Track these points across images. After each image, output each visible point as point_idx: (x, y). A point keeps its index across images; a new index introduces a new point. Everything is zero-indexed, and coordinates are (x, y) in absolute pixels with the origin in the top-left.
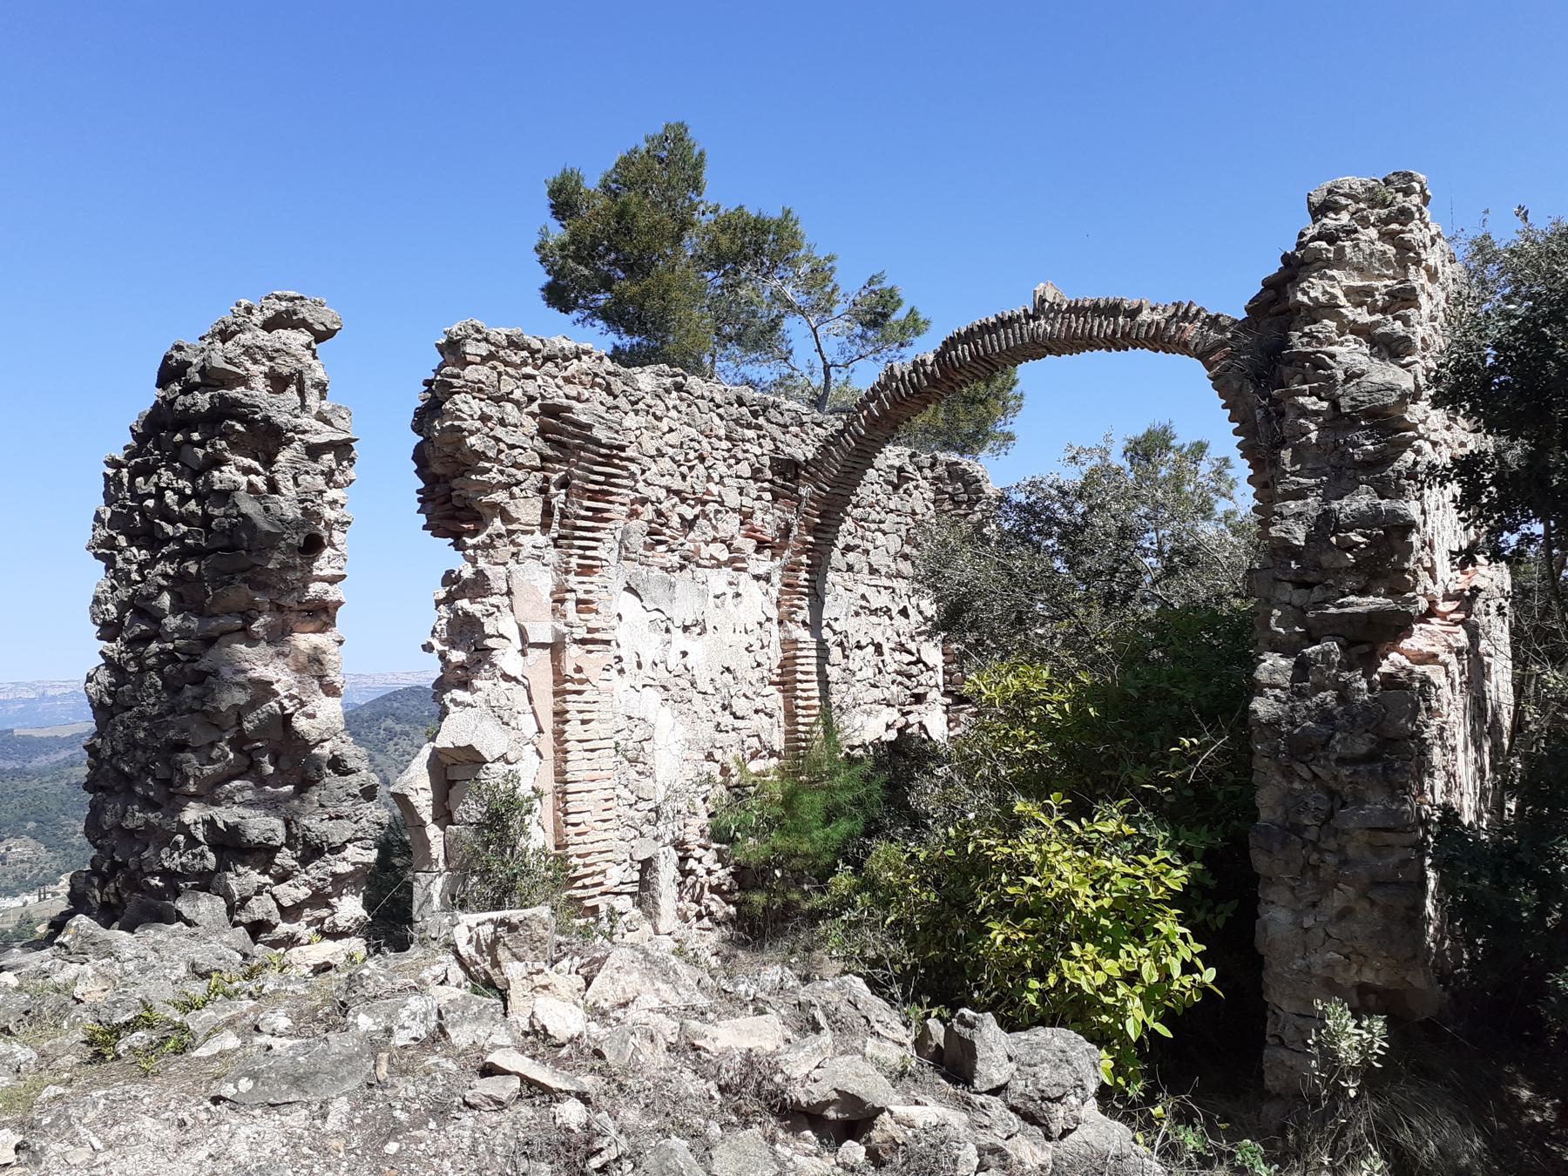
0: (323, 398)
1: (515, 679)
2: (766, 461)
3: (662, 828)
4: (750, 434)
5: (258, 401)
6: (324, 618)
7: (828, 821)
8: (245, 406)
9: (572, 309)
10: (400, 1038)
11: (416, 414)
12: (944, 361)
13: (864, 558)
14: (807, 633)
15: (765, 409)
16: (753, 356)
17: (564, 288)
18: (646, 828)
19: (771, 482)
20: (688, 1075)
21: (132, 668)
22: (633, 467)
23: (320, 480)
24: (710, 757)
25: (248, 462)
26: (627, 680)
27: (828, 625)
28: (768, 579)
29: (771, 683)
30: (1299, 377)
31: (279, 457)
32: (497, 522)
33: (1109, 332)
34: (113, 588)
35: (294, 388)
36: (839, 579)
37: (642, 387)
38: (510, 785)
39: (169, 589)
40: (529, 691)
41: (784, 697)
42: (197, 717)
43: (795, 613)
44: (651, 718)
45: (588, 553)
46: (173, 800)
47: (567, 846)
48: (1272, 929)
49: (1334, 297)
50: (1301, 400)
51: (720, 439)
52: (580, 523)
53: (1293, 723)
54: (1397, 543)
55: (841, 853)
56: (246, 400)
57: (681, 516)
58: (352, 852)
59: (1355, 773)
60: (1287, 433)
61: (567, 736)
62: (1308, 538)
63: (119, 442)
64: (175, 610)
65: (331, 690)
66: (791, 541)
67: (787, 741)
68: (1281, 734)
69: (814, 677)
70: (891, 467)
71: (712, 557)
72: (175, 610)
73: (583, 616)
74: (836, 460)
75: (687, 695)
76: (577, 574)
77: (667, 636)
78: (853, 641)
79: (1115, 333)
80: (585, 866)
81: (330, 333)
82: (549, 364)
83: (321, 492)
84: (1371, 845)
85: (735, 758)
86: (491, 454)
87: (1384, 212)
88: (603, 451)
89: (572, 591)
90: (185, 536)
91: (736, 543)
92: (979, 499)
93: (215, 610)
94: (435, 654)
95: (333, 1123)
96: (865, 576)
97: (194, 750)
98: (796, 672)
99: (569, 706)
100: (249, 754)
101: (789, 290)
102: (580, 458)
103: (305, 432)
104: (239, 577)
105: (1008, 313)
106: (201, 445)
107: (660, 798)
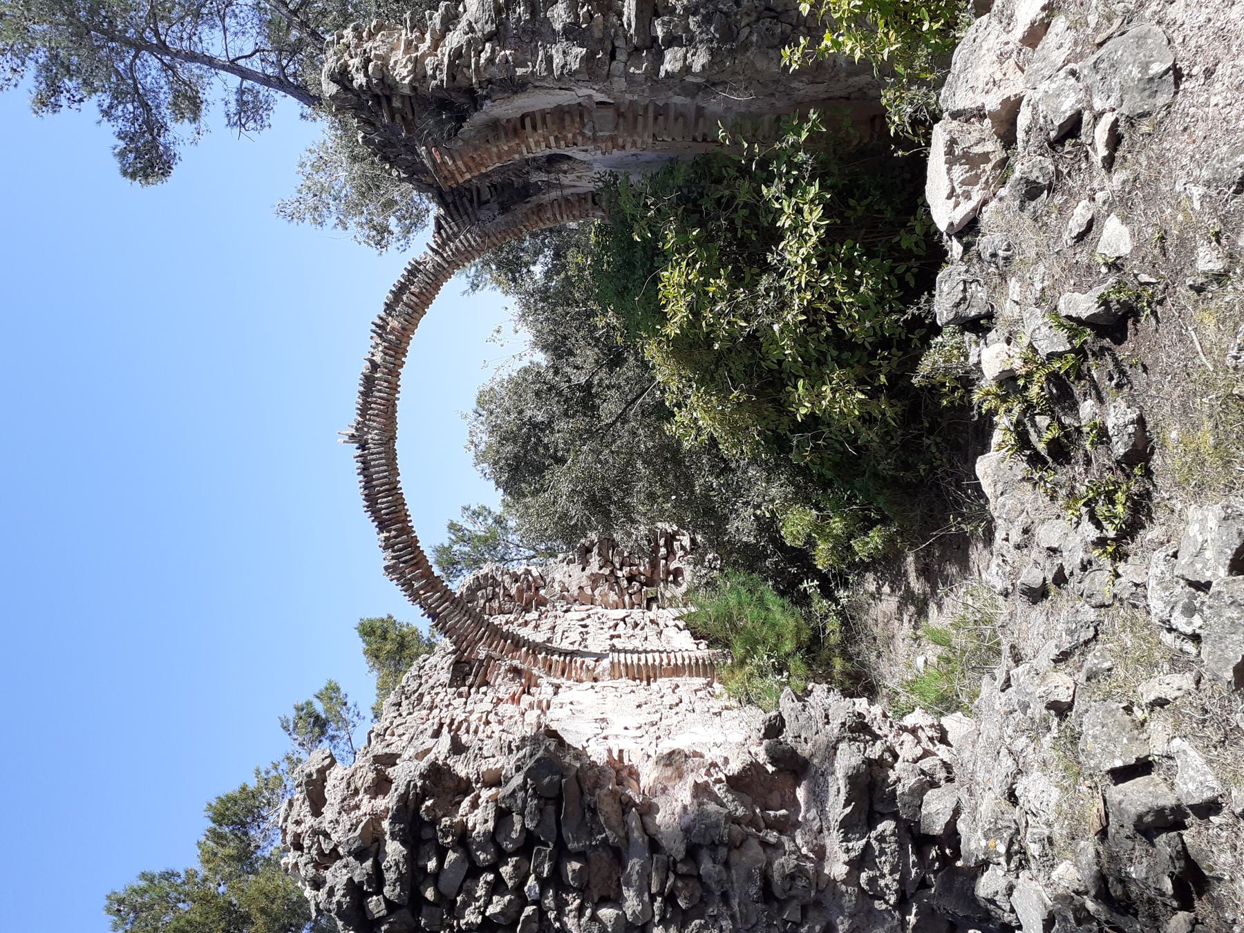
8: (407, 792)
12: (390, 520)
19: (470, 687)
28: (558, 687)
30: (465, 70)
31: (463, 774)
33: (386, 384)
39: (597, 906)
41: (661, 677)
43: (587, 667)
53: (711, 41)
64: (616, 900)
66: (524, 667)
67: (698, 675)
72: (616, 900)
74: (458, 621)
92: (493, 577)
93: (622, 834)
98: (638, 665)
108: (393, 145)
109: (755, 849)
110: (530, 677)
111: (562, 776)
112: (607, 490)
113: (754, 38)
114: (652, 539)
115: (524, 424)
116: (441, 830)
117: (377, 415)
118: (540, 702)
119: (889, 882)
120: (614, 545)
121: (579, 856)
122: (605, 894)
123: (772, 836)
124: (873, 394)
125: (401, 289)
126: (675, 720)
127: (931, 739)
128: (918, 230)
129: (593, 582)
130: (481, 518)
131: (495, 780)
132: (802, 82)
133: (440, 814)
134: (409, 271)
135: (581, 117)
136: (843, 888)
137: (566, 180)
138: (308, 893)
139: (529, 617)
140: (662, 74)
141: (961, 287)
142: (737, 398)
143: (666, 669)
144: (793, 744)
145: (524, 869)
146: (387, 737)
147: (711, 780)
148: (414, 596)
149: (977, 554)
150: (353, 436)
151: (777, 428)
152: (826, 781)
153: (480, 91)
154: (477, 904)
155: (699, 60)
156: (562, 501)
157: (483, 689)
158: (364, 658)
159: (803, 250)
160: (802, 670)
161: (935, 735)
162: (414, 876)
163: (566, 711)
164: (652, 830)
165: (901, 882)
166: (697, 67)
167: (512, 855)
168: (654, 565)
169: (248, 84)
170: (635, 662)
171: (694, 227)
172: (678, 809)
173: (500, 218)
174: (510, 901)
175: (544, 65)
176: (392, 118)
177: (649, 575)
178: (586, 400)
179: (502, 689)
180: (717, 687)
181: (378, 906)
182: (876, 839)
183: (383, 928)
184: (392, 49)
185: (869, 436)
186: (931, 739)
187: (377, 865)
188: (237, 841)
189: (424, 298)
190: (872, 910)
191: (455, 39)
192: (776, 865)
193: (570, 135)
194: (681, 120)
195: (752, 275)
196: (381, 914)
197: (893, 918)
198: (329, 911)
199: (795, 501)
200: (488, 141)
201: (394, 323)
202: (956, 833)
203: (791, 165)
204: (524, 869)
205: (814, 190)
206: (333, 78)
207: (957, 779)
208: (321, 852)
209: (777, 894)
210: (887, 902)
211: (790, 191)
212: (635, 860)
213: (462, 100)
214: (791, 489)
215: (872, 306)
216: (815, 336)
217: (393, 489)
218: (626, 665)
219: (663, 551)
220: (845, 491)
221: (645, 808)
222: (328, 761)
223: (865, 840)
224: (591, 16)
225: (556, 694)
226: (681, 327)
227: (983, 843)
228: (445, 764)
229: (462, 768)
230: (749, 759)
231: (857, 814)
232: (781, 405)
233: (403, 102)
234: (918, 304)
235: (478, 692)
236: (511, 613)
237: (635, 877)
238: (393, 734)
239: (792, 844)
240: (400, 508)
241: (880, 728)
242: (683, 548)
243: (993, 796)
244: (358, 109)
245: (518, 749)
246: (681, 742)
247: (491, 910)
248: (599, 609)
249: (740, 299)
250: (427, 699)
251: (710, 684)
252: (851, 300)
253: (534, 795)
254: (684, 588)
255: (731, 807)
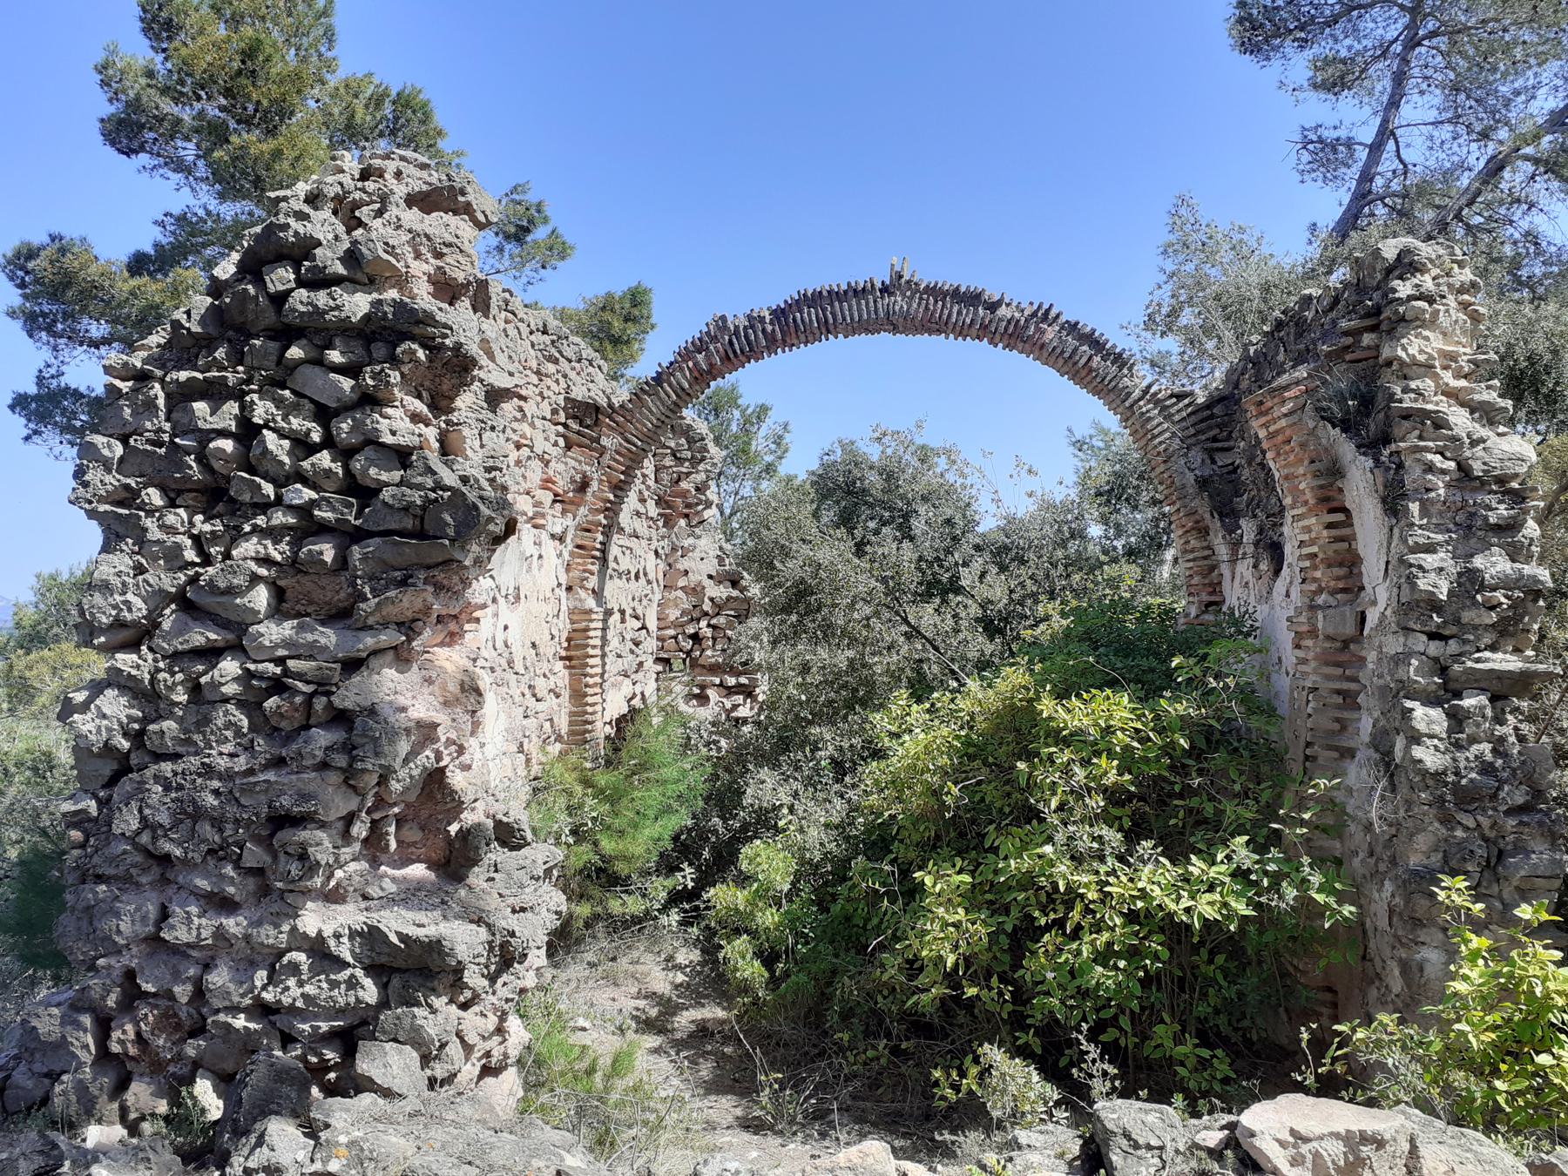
8: (436, 324)
19: (565, 425)
28: (561, 539)
30: (1417, 432)
31: (459, 403)
33: (968, 321)
39: (273, 585)
53: (1457, 774)
59: (1521, 823)
62: (1451, 593)
64: (281, 606)
67: (571, 723)
68: (1446, 784)
72: (281, 606)
92: (703, 459)
93: (371, 621)
108: (1299, 335)
109: (342, 804)
110: (577, 504)
111: (452, 541)
112: (819, 610)
113: (1459, 833)
114: (747, 667)
115: (909, 504)
116: (382, 370)
117: (927, 308)
118: (543, 516)
119: (292, 993)
120: (742, 617)
121: (342, 561)
122: (289, 594)
123: (360, 830)
124: (952, 979)
125: (1096, 344)
126: (516, 693)
127: (488, 1054)
128: (1181, 1049)
129: (694, 589)
130: (773, 447)
131: (447, 449)
132: (1393, 896)
133: (405, 369)
134: (1120, 355)
135: (1344, 590)
136: (286, 928)
137: (1244, 568)
138: (302, 188)
139: (651, 504)
140: (1409, 704)
141: (1155, 1142)
142: (948, 793)
143: (580, 681)
144: (486, 861)
145: (327, 484)
146: (504, 314)
147: (440, 746)
148: (685, 354)
149: (726, 1107)
150: (901, 277)
151: (901, 841)
152: (434, 907)
153: (1386, 452)
154: (279, 418)
155: (1429, 757)
156: (805, 550)
157: (561, 442)
158: (602, 293)
159: (1157, 892)
160: (577, 863)
161: (494, 1060)
162: (319, 331)
163: (530, 549)
164: (374, 662)
165: (292, 1009)
166: (1418, 752)
167: (346, 468)
168: (714, 669)
169: (1362, 154)
170: (591, 642)
171: (1190, 738)
172: (402, 700)
173: (1190, 477)
174: (282, 463)
175: (1421, 541)
176: (1346, 333)
177: (701, 661)
178: (940, 588)
179: (561, 467)
180: (555, 749)
181: (281, 280)
182: (353, 976)
183: (250, 287)
184: (1444, 334)
185: (891, 966)
186: (488, 1054)
187: (337, 281)
188: (373, 124)
189: (1083, 373)
190: (253, 965)
191: (1460, 420)
192: (321, 835)
193: (1318, 574)
194: (1337, 726)
195: (1120, 818)
196: (270, 285)
197: (243, 996)
198: (276, 214)
199: (802, 861)
200: (1313, 462)
201: (1051, 333)
202: (358, 1091)
203: (1276, 879)
204: (327, 484)
205: (1241, 908)
206: (1404, 253)
207: (433, 1094)
208: (357, 205)
209: (280, 835)
210: (264, 988)
211: (1240, 874)
212: (333, 638)
213: (1373, 427)
214: (817, 856)
215: (1077, 982)
216: (1033, 900)
217: (827, 328)
218: (587, 630)
219: (731, 681)
220: (812, 929)
221: (405, 654)
222: (482, 218)
223: (351, 961)
224: (1492, 608)
225: (553, 536)
226: (1050, 718)
227: (343, 1139)
228: (473, 379)
229: (467, 402)
230: (467, 799)
231: (387, 950)
232: (934, 847)
233: (1369, 348)
234: (1102, 1060)
235: (558, 435)
236: (656, 481)
237: (310, 637)
238: (507, 322)
239: (348, 857)
240: (802, 337)
241: (505, 984)
242: (735, 707)
243: (409, 1154)
244: (1358, 287)
245: (492, 481)
246: (491, 706)
247: (270, 437)
248: (658, 596)
249: (1087, 800)
250: (551, 368)
251: (559, 738)
252: (1085, 954)
253: (426, 499)
254: (683, 707)
255: (402, 774)
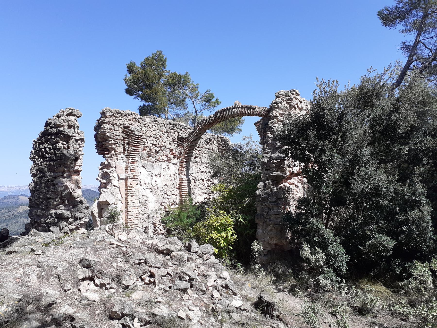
0: (78, 129)
1: (117, 186)
2: (176, 137)
3: (150, 220)
4: (172, 131)
5: (66, 131)
6: (78, 173)
7: (187, 219)
8: (63, 132)
9: (133, 95)
10: (98, 240)
11: (95, 127)
13: (200, 159)
14: (185, 177)
15: (176, 125)
16: (178, 108)
17: (131, 90)
18: (146, 220)
19: (177, 142)
20: (143, 246)
21: (39, 183)
22: (144, 140)
23: (78, 146)
24: (161, 205)
25: (64, 142)
26: (142, 187)
27: (191, 175)
28: (176, 165)
29: (177, 188)
31: (70, 142)
32: (113, 152)
34: (35, 167)
35: (73, 128)
36: (194, 164)
37: (147, 121)
38: (115, 209)
40: (120, 189)
42: (53, 192)
44: (148, 196)
45: (133, 159)
46: (48, 208)
47: (128, 223)
48: (258, 233)
49: (277, 115)
50: (268, 135)
51: (165, 132)
52: (131, 152)
54: (282, 162)
55: (190, 226)
56: (63, 131)
57: (156, 150)
58: (84, 219)
60: (266, 141)
61: (128, 199)
62: (268, 161)
63: (36, 137)
65: (79, 188)
66: (182, 156)
67: (180, 201)
69: (187, 187)
70: (208, 138)
71: (163, 159)
72: (49, 171)
73: (132, 173)
75: (156, 190)
76: (131, 163)
77: (152, 177)
78: (197, 179)
79: (250, 113)
80: (132, 227)
81: (80, 116)
82: (125, 117)
83: (78, 149)
84: (275, 218)
85: (167, 205)
86: (112, 137)
87: (287, 98)
88: (137, 137)
89: (130, 167)
90: (51, 157)
91: (169, 156)
93: (57, 172)
94: (99, 181)
95: (88, 250)
96: (200, 163)
97: (52, 199)
99: (128, 193)
100: (63, 200)
101: (187, 92)
102: (132, 138)
103: (75, 137)
104: (62, 165)
105: (229, 107)
106: (54, 139)
107: (149, 213)
145: (53, 154)
202: (49, 232)
